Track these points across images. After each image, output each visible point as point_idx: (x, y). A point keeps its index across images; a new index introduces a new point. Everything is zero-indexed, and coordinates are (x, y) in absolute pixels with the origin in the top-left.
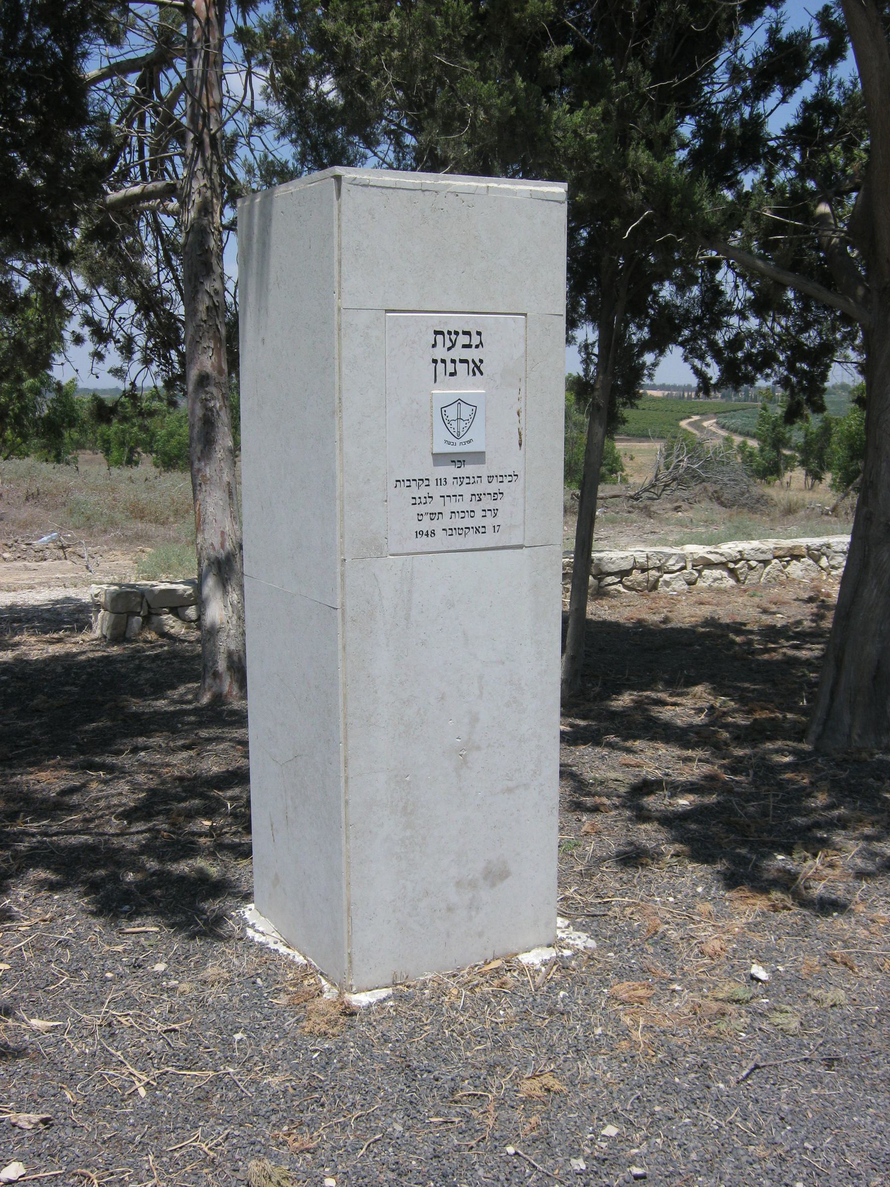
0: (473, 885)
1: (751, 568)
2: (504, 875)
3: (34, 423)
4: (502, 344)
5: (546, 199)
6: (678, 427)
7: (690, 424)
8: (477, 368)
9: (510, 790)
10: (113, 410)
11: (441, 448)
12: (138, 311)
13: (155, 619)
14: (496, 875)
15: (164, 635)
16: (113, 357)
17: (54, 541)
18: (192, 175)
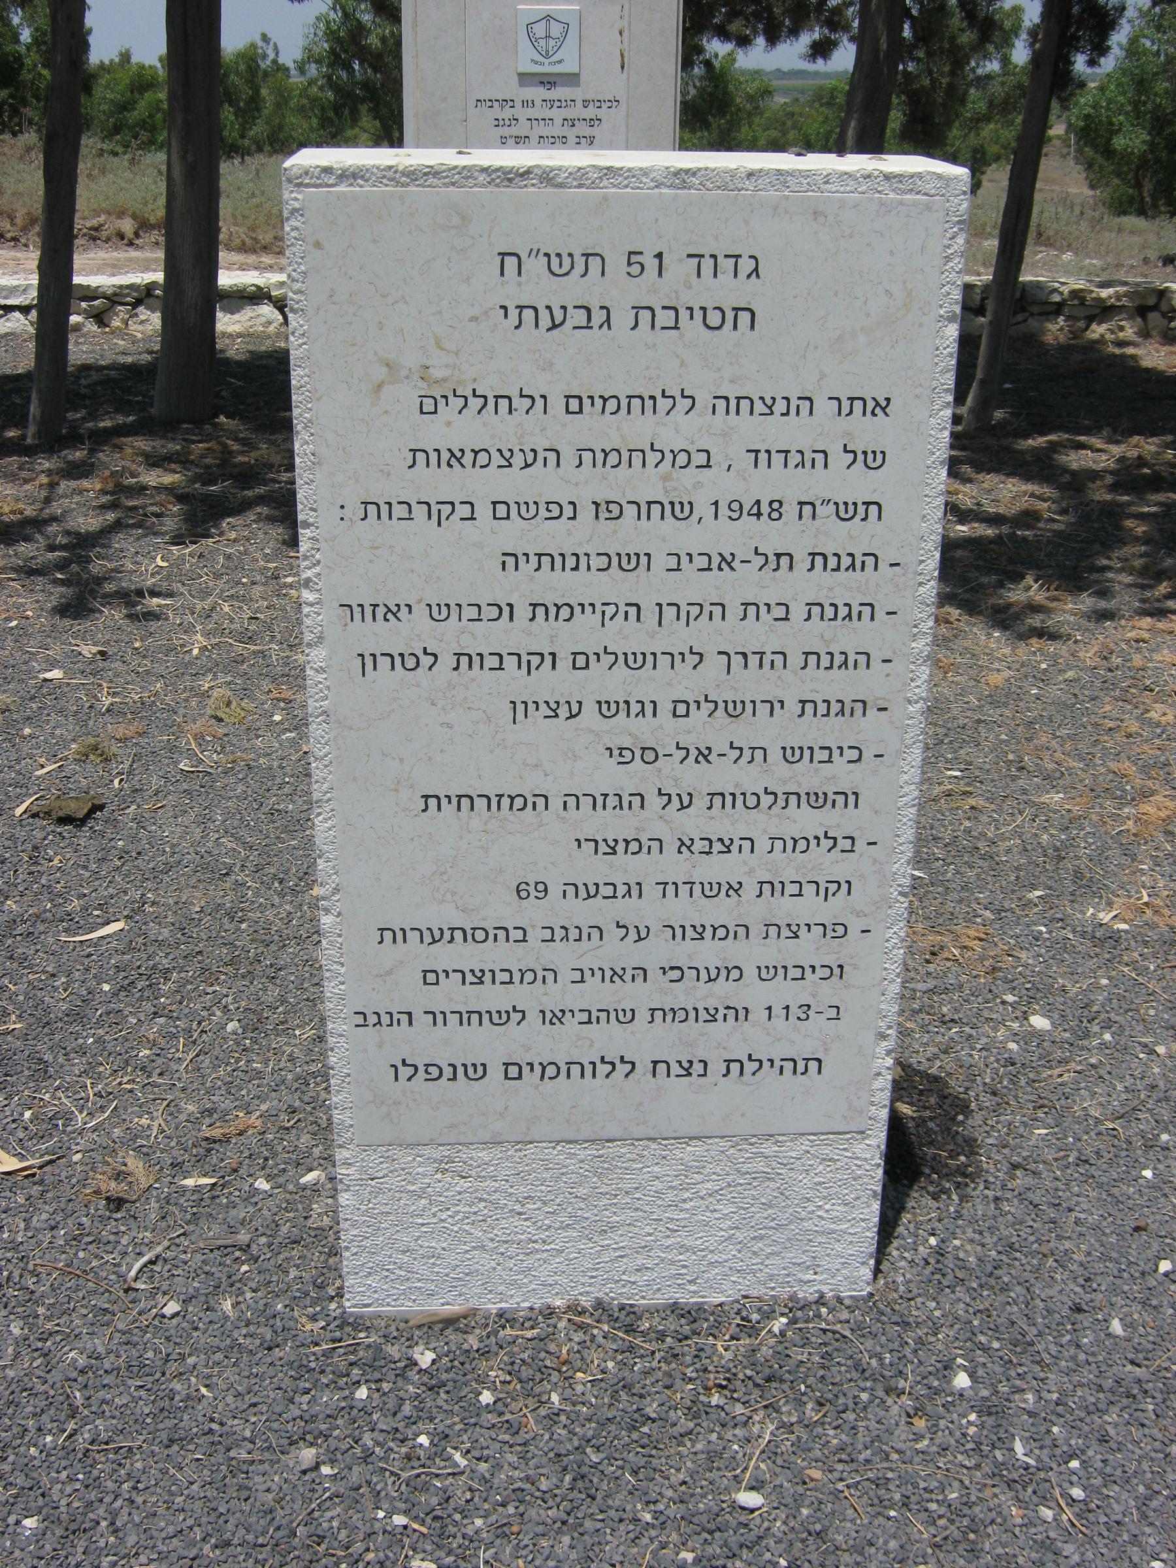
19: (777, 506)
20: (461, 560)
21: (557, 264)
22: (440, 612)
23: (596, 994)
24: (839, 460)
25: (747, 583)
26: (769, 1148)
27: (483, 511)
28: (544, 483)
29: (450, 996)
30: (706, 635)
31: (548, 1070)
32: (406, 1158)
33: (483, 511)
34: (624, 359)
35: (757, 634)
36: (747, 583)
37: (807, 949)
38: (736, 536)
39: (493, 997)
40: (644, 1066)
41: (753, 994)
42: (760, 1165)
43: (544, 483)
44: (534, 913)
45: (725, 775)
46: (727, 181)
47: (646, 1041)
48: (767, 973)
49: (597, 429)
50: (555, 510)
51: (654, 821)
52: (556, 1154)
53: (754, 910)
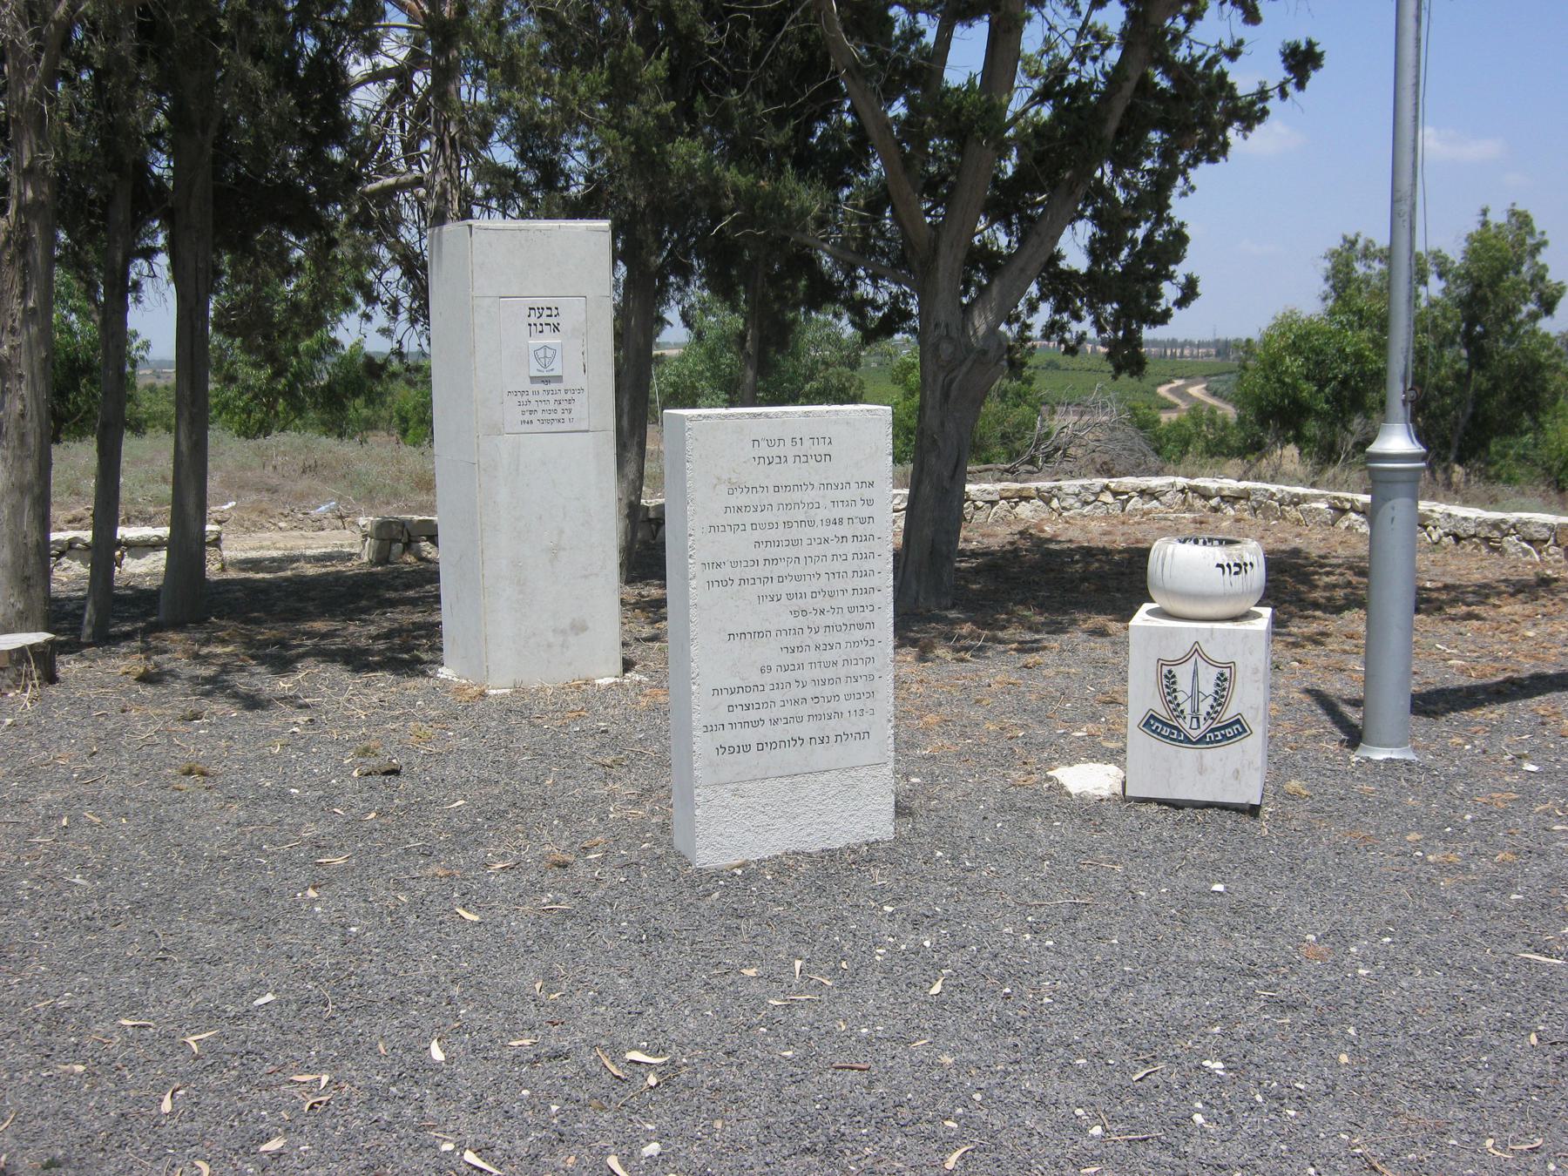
0: (563, 632)
1: (977, 508)
2: (584, 628)
3: (312, 393)
4: (572, 314)
5: (597, 230)
6: (1155, 394)
7: (1171, 391)
8: (556, 328)
9: (586, 577)
10: (383, 367)
11: (535, 373)
12: (403, 274)
13: (414, 545)
14: (579, 628)
15: (422, 559)
16: (380, 316)
17: (332, 511)
18: (435, 171)
19: (841, 520)
20: (739, 545)
21: (770, 443)
22: (735, 564)
23: (790, 711)
24: (860, 503)
25: (833, 548)
26: (853, 773)
27: (748, 527)
28: (768, 516)
29: (739, 715)
30: (821, 567)
31: (773, 745)
32: (721, 791)
33: (748, 527)
34: (790, 473)
35: (838, 566)
36: (833, 548)
37: (860, 687)
38: (830, 531)
39: (753, 715)
40: (807, 740)
41: (844, 706)
42: (850, 781)
43: (768, 516)
44: (768, 678)
45: (830, 619)
46: (820, 415)
47: (807, 729)
48: (848, 697)
49: (784, 497)
50: (771, 526)
51: (807, 638)
52: (776, 783)
53: (842, 671)
